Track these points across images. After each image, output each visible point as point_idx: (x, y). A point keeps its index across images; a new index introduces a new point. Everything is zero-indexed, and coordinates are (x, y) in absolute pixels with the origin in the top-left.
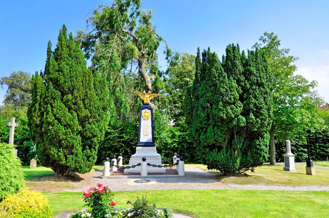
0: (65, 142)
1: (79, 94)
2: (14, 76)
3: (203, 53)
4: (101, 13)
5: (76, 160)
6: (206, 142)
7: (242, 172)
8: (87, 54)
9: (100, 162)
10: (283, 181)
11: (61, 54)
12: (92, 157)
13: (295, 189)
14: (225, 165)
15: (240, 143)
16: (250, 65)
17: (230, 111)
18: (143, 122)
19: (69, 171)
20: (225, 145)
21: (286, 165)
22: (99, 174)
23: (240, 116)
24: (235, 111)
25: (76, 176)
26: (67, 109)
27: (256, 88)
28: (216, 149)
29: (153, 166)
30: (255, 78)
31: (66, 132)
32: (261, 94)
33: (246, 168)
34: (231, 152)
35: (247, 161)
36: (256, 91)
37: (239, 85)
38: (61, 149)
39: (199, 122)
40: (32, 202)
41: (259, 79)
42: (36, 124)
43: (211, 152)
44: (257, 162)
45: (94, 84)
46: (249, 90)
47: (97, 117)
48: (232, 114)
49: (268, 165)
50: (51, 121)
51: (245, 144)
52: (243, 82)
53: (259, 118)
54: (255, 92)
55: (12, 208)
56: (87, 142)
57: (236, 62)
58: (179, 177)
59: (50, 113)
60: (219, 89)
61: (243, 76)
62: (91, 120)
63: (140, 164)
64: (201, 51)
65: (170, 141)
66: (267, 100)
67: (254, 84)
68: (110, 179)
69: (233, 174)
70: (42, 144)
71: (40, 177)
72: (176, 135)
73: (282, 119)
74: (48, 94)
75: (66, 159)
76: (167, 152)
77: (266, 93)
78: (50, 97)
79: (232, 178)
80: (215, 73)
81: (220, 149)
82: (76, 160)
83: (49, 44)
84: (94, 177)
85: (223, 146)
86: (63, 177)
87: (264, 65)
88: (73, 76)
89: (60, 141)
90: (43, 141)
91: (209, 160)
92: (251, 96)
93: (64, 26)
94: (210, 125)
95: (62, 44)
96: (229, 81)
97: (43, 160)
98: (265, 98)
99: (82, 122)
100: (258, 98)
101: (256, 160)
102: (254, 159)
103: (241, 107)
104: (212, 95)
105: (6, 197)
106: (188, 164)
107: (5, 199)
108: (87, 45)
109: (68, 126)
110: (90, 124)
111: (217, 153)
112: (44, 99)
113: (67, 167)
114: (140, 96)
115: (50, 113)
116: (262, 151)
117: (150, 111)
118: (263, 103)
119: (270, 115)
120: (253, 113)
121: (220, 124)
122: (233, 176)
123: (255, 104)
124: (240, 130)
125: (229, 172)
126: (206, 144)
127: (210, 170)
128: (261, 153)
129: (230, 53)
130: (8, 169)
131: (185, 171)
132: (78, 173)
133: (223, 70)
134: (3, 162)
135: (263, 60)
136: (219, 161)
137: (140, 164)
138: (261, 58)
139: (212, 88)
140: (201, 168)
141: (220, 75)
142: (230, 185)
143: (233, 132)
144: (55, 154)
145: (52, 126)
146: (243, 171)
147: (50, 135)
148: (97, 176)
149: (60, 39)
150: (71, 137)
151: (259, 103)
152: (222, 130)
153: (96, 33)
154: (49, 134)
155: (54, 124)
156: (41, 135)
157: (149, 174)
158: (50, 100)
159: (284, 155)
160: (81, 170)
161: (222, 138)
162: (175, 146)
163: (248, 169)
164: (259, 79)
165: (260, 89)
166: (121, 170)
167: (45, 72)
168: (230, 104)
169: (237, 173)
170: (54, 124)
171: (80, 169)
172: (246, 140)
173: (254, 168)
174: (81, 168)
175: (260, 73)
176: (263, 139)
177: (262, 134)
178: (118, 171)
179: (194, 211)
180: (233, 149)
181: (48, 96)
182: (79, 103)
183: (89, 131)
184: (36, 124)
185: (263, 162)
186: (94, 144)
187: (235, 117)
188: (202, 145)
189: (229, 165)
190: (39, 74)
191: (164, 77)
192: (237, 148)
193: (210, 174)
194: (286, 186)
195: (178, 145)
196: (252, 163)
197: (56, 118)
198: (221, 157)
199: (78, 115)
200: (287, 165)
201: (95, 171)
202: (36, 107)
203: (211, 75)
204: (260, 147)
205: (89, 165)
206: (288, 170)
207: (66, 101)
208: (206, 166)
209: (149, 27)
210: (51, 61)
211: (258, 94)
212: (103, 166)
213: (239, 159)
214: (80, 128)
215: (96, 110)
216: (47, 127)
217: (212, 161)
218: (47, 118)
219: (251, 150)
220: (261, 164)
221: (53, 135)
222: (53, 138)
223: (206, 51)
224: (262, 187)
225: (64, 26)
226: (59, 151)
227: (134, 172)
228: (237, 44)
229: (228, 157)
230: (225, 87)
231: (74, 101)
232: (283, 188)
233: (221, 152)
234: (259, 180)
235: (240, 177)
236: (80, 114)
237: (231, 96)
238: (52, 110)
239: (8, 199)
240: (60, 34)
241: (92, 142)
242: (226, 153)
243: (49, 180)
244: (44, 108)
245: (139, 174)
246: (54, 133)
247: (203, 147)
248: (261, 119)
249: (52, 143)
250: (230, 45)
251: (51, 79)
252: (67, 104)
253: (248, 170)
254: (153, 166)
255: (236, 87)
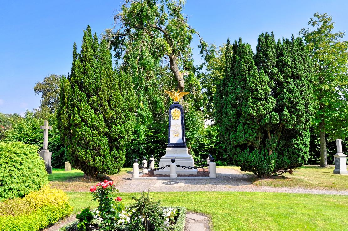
0: (92, 144)
1: (105, 95)
2: (47, 81)
3: (234, 44)
4: (129, 8)
5: (103, 162)
6: (236, 141)
7: (279, 174)
8: (118, 53)
9: (129, 164)
10: (326, 184)
11: (86, 56)
12: (120, 158)
13: (338, 194)
14: (259, 166)
15: (275, 142)
16: (283, 56)
17: (261, 108)
18: (173, 122)
19: (98, 173)
20: (257, 144)
21: (336, 168)
22: (130, 175)
23: (273, 113)
24: (266, 107)
25: (106, 177)
26: (93, 111)
27: (291, 81)
28: (248, 149)
29: (183, 167)
30: (290, 70)
31: (93, 134)
32: (297, 87)
33: (284, 170)
34: (265, 152)
35: (284, 162)
36: (291, 84)
37: (271, 79)
38: (89, 151)
39: (229, 120)
40: (52, 198)
41: (294, 70)
42: (65, 127)
43: (243, 153)
44: (295, 163)
45: (120, 85)
46: (283, 83)
47: (123, 117)
48: (263, 110)
49: (318, 167)
50: (78, 122)
51: (280, 143)
52: (276, 75)
53: (294, 114)
54: (289, 86)
55: (33, 203)
56: (114, 143)
57: (269, 53)
58: (209, 179)
59: (77, 116)
60: (248, 84)
61: (276, 68)
62: (117, 121)
63: (169, 166)
64: (231, 44)
65: (206, 141)
66: (305, 94)
67: (289, 76)
68: (139, 180)
69: (268, 176)
70: (70, 146)
71: (70, 178)
72: (213, 136)
73: (332, 114)
74: (74, 96)
75: (94, 161)
76: (203, 153)
77: (303, 85)
78: (77, 99)
79: (267, 180)
80: (245, 67)
81: (252, 148)
82: (103, 162)
83: (75, 46)
84: (124, 179)
85: (255, 145)
86: (92, 178)
87: (301, 55)
88: (97, 78)
89: (88, 143)
90: (72, 143)
91: (240, 161)
92: (285, 90)
93: (89, 27)
94: (240, 123)
95: (87, 45)
96: (259, 74)
97: (73, 161)
98: (302, 91)
99: (108, 122)
100: (294, 92)
101: (293, 161)
102: (291, 160)
103: (273, 102)
104: (241, 91)
105: (28, 193)
106: (227, 166)
107: (27, 195)
108: (116, 43)
109: (94, 128)
110: (116, 125)
111: (249, 153)
112: (70, 102)
113: (96, 169)
114: (169, 94)
115: (77, 116)
116: (300, 151)
117: (179, 110)
118: (300, 97)
119: (309, 110)
120: (287, 109)
121: (250, 122)
122: (269, 178)
123: (290, 99)
124: (274, 128)
125: (263, 174)
126: (236, 144)
127: (244, 172)
128: (299, 153)
129: (262, 43)
130: (31, 168)
131: (217, 172)
132: (107, 175)
133: (254, 63)
134: (26, 162)
135: (300, 49)
136: (251, 162)
137: (169, 166)
138: (298, 47)
139: (242, 83)
140: (235, 171)
141: (250, 68)
142: (263, 187)
143: (266, 131)
144: (83, 156)
145: (79, 128)
146: (280, 173)
147: (77, 137)
148: (128, 177)
149: (84, 41)
150: (98, 138)
151: (294, 98)
152: (253, 128)
153: (125, 31)
154: (76, 136)
155: (81, 126)
156: (70, 138)
157: (178, 176)
158: (77, 103)
159: (335, 156)
160: (109, 171)
161: (253, 136)
162: (212, 147)
163: (287, 171)
164: (294, 70)
165: (297, 82)
166: (151, 172)
167: (71, 75)
168: (260, 100)
169: (273, 175)
170: (81, 126)
171: (108, 171)
172: (282, 139)
173: (293, 170)
174: (109, 169)
175: (295, 64)
176: (302, 138)
177: (300, 132)
178: (148, 173)
179: (211, 212)
180: (267, 149)
181: (75, 99)
182: (104, 104)
183: (115, 133)
184: (65, 126)
185: (302, 164)
186: (121, 145)
187: (267, 114)
188: (233, 145)
189: (263, 166)
190: (67, 76)
191: (198, 72)
192: (271, 147)
193: (245, 176)
194: (329, 190)
195: (215, 146)
196: (289, 164)
197: (83, 120)
198: (253, 157)
199: (104, 117)
200: (338, 167)
201: (127, 173)
202: (64, 110)
203: (240, 69)
204: (298, 146)
205: (117, 166)
206: (339, 173)
207: (91, 102)
208: (240, 168)
209: (179, 19)
210: (76, 64)
211: (294, 88)
212: (132, 169)
213: (274, 159)
214: (106, 129)
215: (121, 111)
216: (74, 129)
217: (244, 162)
218: (74, 120)
219: (288, 150)
220: (299, 166)
221: (81, 136)
222: (81, 140)
223: (237, 43)
224: (300, 190)
225: (89, 27)
226: (87, 153)
227: (163, 174)
228: (272, 32)
229: (261, 158)
230: (255, 81)
231: (99, 102)
232: (325, 192)
233: (253, 152)
234: (297, 183)
235: (275, 179)
236: (106, 115)
237: (262, 90)
238: (79, 113)
239: (30, 195)
240: (85, 36)
241: (119, 143)
242: (260, 153)
243: (79, 181)
244: (71, 111)
245: (169, 176)
246: (81, 135)
247: (234, 147)
248: (298, 116)
249: (80, 144)
250: (263, 33)
251: (77, 82)
252: (93, 106)
253: (286, 172)
254: (183, 167)
255: (267, 81)
